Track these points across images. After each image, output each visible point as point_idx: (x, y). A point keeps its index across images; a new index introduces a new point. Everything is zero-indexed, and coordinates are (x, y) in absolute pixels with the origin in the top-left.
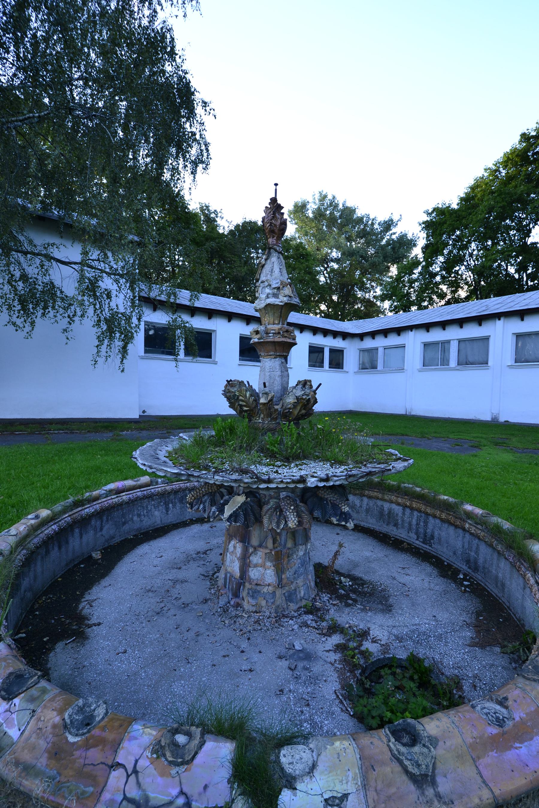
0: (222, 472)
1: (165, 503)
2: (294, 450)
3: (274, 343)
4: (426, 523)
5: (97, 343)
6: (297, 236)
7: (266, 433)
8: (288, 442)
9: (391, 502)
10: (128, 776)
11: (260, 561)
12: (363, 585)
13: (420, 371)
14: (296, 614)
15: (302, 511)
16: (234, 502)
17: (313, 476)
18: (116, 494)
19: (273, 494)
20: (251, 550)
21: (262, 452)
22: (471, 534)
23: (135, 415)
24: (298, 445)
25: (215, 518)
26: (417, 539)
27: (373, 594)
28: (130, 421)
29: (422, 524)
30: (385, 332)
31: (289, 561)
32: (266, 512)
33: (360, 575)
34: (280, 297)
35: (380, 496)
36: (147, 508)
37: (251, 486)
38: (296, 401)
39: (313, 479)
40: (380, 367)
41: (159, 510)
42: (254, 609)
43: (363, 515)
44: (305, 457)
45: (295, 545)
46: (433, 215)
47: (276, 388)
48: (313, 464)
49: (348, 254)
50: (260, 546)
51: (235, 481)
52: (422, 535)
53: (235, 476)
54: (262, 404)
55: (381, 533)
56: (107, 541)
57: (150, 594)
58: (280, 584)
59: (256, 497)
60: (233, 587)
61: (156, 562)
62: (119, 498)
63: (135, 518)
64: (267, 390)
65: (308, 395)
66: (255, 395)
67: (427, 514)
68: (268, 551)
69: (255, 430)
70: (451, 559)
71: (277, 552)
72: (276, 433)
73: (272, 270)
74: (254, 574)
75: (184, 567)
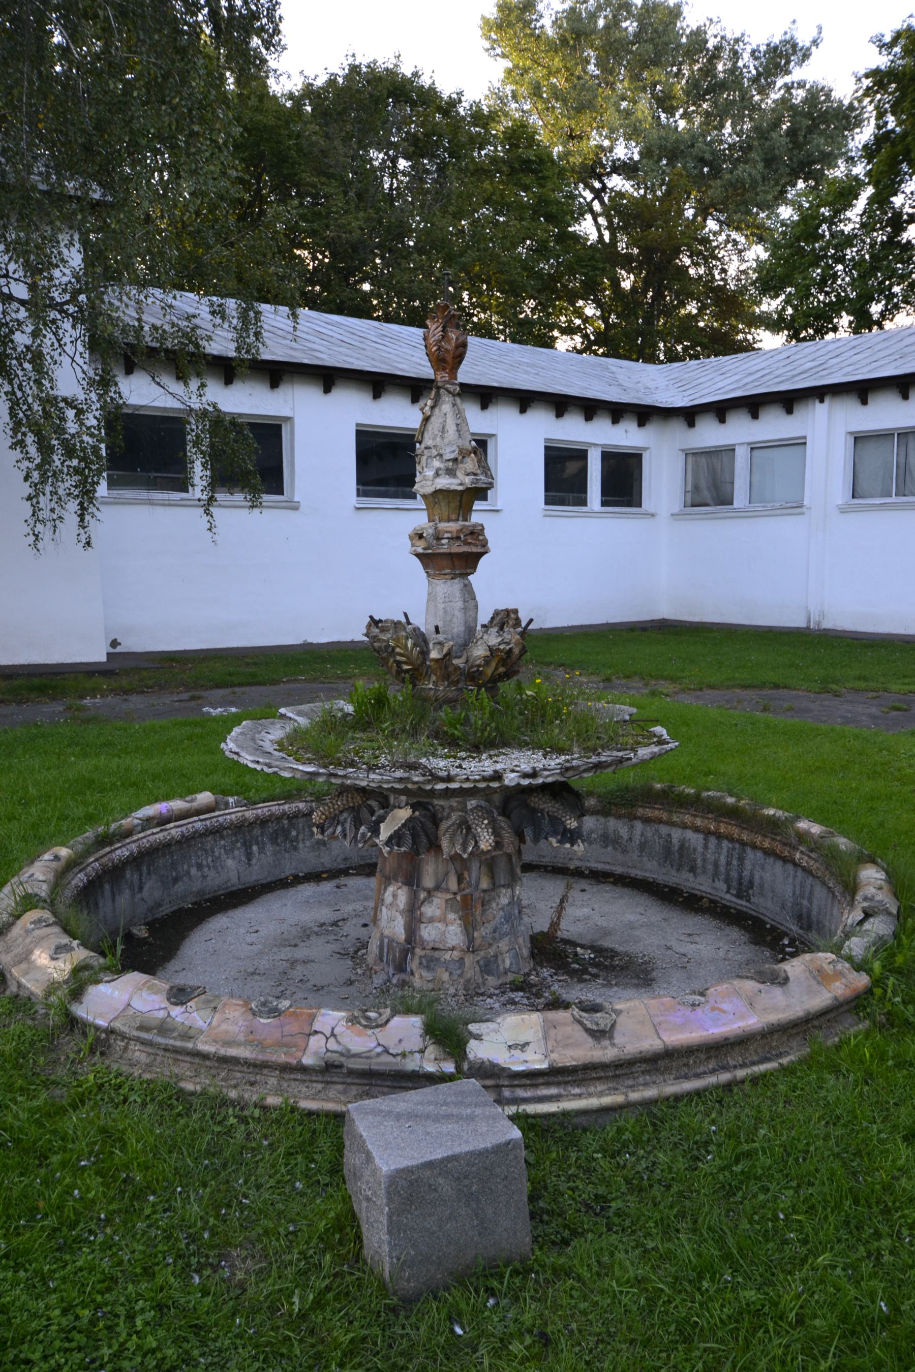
0: (379, 768)
1: (244, 844)
2: (486, 734)
3: (451, 555)
4: (741, 859)
5: (27, 490)
6: (509, 89)
7: (441, 707)
8: (476, 718)
9: (685, 827)
10: (327, 1039)
11: (438, 913)
12: (612, 957)
13: (844, 510)
14: (497, 992)
15: (502, 828)
16: (393, 819)
17: (513, 771)
18: (159, 824)
19: (455, 804)
20: (423, 895)
21: (436, 738)
22: (804, 869)
23: (97, 654)
24: (493, 725)
25: (365, 842)
26: (728, 892)
27: (627, 968)
28: (89, 671)
29: (735, 862)
30: (753, 405)
31: (484, 911)
32: (446, 831)
33: (610, 946)
34: (459, 474)
35: (665, 816)
36: (213, 852)
37: (423, 786)
38: (488, 653)
39: (513, 775)
40: (740, 498)
41: (234, 858)
42: (430, 986)
43: (635, 856)
44: (506, 744)
45: (494, 887)
46: (897, 49)
47: (455, 631)
48: (516, 754)
49: (662, 150)
50: (437, 888)
51: (401, 780)
52: (735, 884)
53: (399, 773)
54: (433, 660)
55: (666, 886)
56: (150, 910)
57: (256, 977)
58: (471, 947)
59: (428, 810)
60: (394, 956)
61: (251, 938)
62: (166, 833)
63: (194, 871)
64: (441, 637)
65: (508, 644)
66: (421, 639)
67: (743, 844)
68: (450, 896)
69: (421, 702)
70: (777, 918)
71: (465, 896)
72: (458, 706)
73: (443, 428)
74: (428, 933)
75: (302, 944)
